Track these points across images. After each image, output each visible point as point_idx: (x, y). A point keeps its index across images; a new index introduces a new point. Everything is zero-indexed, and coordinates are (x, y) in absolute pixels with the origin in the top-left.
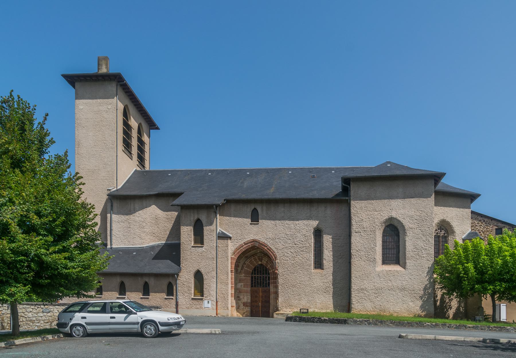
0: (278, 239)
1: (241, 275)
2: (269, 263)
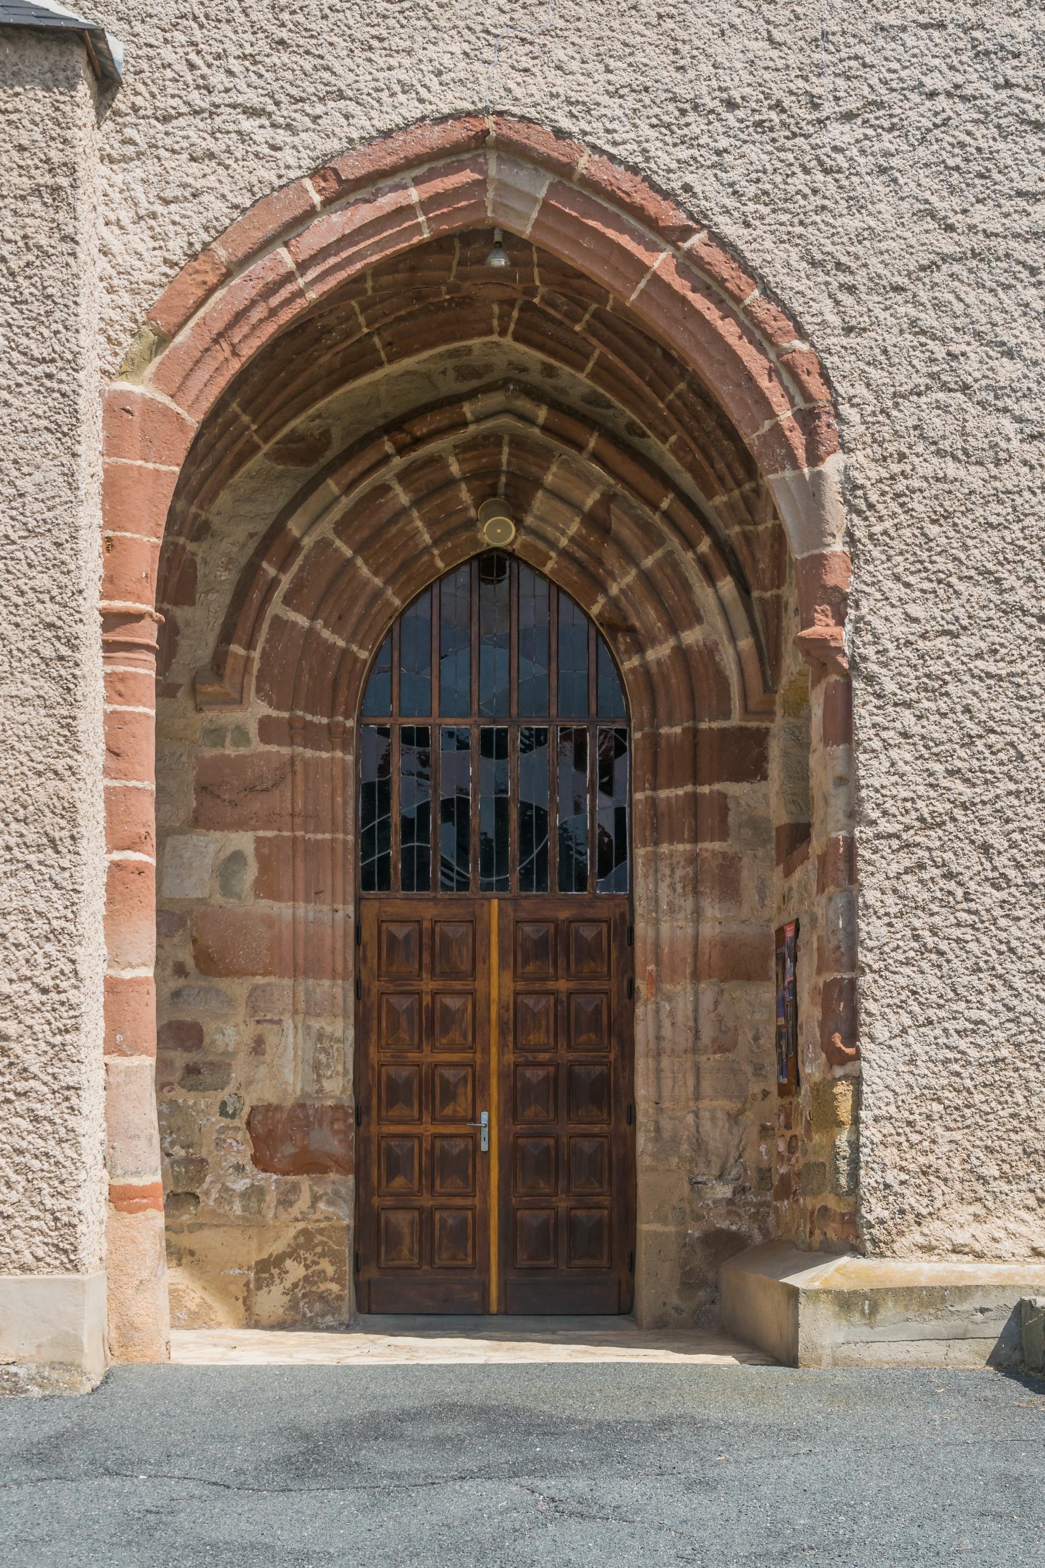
0: (848, 117)
1: (231, 717)
2: (626, 532)
